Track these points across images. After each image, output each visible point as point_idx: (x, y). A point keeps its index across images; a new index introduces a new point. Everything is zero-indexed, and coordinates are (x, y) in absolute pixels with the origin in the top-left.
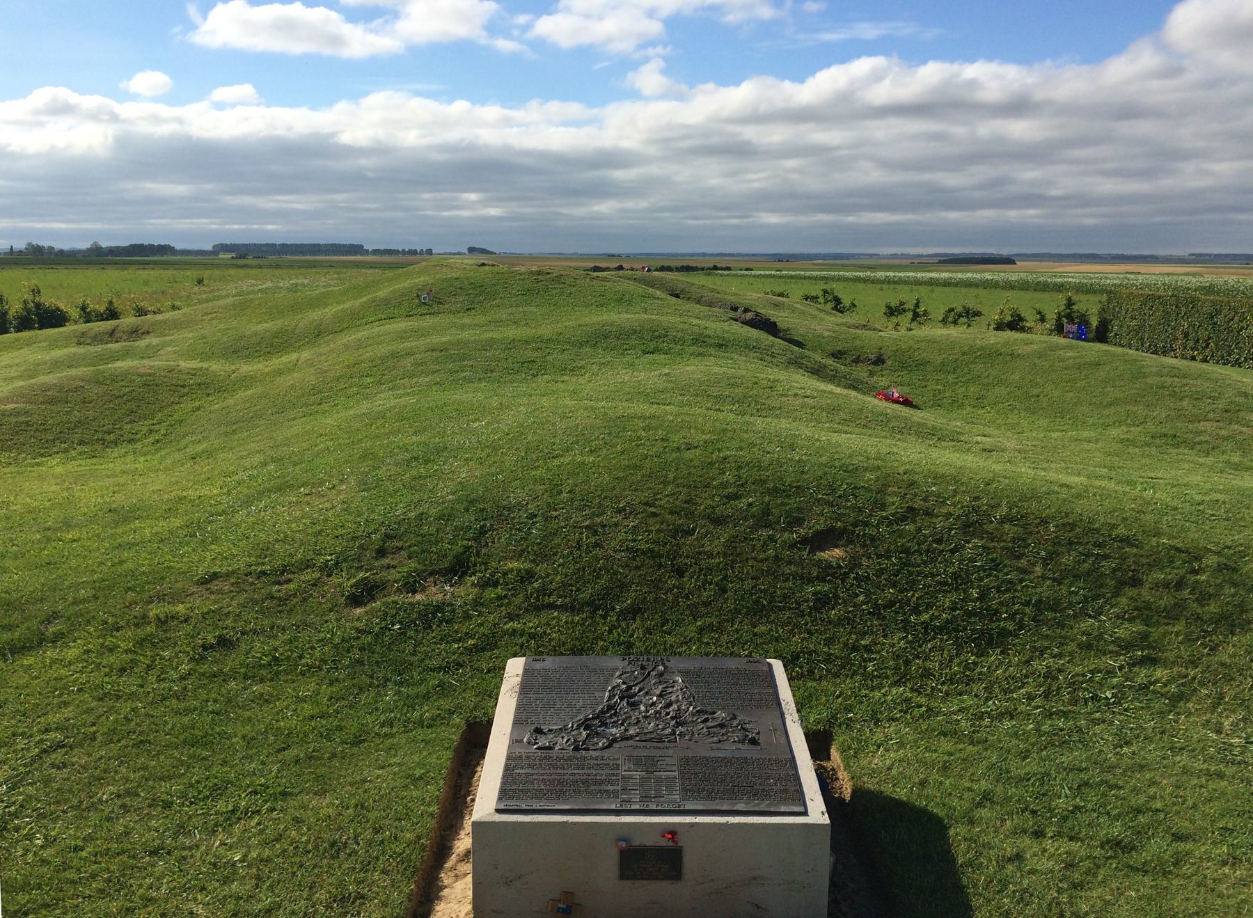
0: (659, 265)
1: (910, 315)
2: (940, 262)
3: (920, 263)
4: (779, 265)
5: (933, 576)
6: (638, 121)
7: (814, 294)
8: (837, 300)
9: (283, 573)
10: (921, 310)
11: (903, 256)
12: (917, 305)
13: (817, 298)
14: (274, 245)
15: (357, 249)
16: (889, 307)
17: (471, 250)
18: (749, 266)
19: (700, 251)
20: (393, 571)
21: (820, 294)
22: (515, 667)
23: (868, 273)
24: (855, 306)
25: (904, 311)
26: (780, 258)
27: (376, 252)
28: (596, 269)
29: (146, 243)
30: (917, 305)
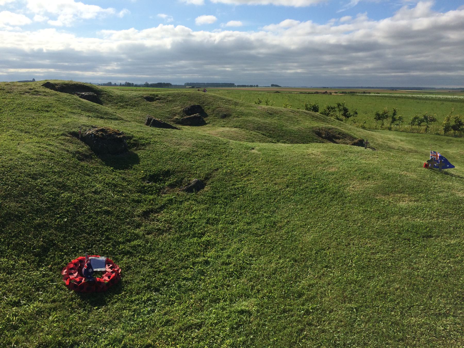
0: (341, 91)
1: (390, 120)
2: (461, 91)
3: (454, 91)
4: (393, 92)
5: (442, 236)
6: (289, 35)
7: (333, 106)
8: (346, 110)
9: (276, 163)
10: (397, 117)
11: (446, 89)
12: (394, 114)
13: (334, 108)
14: (204, 84)
15: (232, 85)
16: (378, 114)
17: (272, 85)
18: (378, 92)
19: (347, 86)
20: (136, 198)
21: (336, 106)
22: (94, 270)
23: (421, 95)
24: (356, 113)
25: (387, 116)
26: (392, 89)
27: (238, 86)
28: (364, 93)
29: (196, 82)
30: (394, 114)
